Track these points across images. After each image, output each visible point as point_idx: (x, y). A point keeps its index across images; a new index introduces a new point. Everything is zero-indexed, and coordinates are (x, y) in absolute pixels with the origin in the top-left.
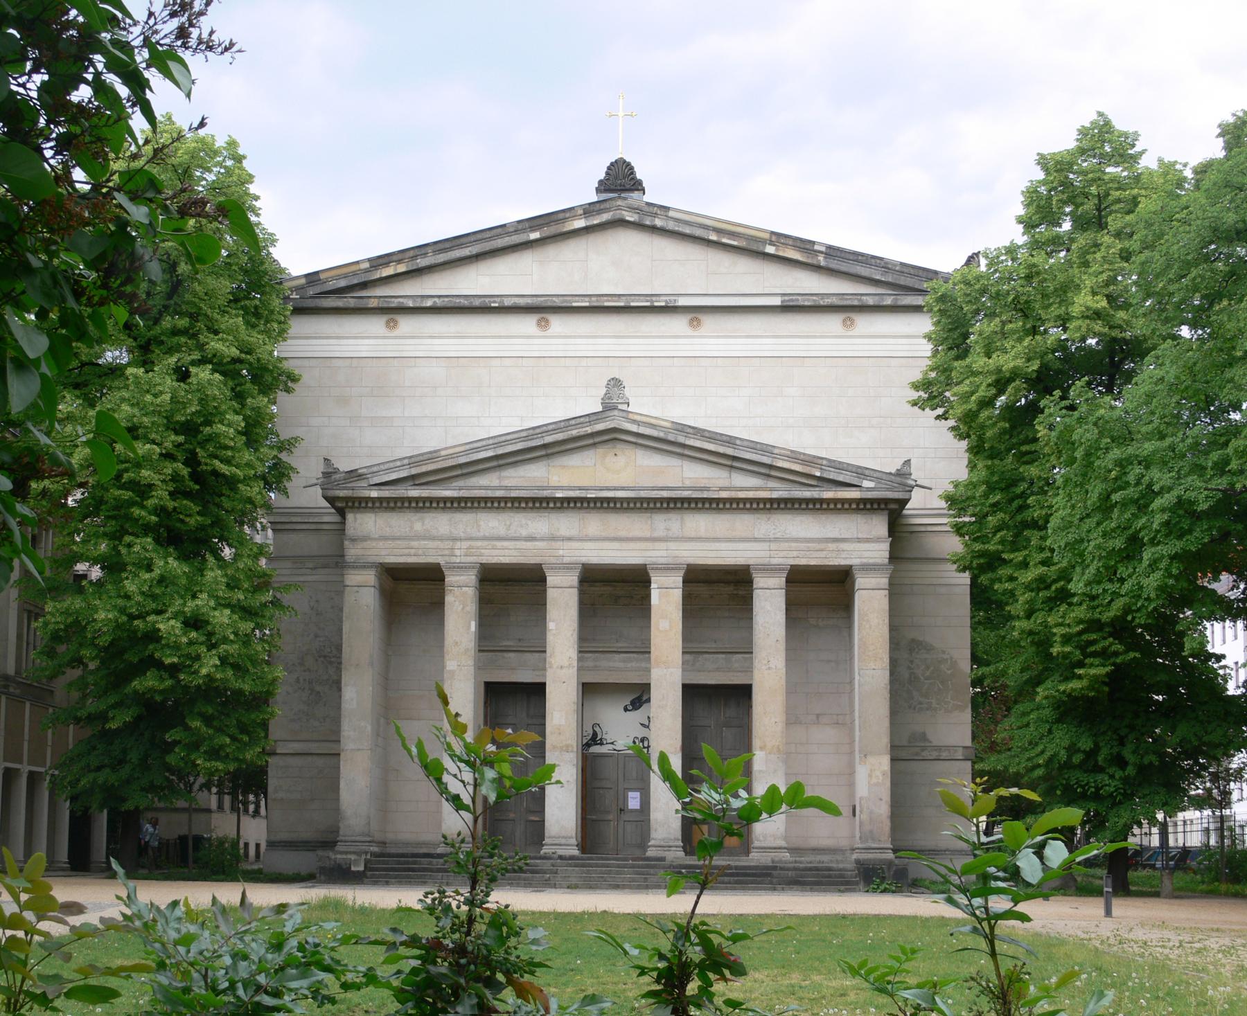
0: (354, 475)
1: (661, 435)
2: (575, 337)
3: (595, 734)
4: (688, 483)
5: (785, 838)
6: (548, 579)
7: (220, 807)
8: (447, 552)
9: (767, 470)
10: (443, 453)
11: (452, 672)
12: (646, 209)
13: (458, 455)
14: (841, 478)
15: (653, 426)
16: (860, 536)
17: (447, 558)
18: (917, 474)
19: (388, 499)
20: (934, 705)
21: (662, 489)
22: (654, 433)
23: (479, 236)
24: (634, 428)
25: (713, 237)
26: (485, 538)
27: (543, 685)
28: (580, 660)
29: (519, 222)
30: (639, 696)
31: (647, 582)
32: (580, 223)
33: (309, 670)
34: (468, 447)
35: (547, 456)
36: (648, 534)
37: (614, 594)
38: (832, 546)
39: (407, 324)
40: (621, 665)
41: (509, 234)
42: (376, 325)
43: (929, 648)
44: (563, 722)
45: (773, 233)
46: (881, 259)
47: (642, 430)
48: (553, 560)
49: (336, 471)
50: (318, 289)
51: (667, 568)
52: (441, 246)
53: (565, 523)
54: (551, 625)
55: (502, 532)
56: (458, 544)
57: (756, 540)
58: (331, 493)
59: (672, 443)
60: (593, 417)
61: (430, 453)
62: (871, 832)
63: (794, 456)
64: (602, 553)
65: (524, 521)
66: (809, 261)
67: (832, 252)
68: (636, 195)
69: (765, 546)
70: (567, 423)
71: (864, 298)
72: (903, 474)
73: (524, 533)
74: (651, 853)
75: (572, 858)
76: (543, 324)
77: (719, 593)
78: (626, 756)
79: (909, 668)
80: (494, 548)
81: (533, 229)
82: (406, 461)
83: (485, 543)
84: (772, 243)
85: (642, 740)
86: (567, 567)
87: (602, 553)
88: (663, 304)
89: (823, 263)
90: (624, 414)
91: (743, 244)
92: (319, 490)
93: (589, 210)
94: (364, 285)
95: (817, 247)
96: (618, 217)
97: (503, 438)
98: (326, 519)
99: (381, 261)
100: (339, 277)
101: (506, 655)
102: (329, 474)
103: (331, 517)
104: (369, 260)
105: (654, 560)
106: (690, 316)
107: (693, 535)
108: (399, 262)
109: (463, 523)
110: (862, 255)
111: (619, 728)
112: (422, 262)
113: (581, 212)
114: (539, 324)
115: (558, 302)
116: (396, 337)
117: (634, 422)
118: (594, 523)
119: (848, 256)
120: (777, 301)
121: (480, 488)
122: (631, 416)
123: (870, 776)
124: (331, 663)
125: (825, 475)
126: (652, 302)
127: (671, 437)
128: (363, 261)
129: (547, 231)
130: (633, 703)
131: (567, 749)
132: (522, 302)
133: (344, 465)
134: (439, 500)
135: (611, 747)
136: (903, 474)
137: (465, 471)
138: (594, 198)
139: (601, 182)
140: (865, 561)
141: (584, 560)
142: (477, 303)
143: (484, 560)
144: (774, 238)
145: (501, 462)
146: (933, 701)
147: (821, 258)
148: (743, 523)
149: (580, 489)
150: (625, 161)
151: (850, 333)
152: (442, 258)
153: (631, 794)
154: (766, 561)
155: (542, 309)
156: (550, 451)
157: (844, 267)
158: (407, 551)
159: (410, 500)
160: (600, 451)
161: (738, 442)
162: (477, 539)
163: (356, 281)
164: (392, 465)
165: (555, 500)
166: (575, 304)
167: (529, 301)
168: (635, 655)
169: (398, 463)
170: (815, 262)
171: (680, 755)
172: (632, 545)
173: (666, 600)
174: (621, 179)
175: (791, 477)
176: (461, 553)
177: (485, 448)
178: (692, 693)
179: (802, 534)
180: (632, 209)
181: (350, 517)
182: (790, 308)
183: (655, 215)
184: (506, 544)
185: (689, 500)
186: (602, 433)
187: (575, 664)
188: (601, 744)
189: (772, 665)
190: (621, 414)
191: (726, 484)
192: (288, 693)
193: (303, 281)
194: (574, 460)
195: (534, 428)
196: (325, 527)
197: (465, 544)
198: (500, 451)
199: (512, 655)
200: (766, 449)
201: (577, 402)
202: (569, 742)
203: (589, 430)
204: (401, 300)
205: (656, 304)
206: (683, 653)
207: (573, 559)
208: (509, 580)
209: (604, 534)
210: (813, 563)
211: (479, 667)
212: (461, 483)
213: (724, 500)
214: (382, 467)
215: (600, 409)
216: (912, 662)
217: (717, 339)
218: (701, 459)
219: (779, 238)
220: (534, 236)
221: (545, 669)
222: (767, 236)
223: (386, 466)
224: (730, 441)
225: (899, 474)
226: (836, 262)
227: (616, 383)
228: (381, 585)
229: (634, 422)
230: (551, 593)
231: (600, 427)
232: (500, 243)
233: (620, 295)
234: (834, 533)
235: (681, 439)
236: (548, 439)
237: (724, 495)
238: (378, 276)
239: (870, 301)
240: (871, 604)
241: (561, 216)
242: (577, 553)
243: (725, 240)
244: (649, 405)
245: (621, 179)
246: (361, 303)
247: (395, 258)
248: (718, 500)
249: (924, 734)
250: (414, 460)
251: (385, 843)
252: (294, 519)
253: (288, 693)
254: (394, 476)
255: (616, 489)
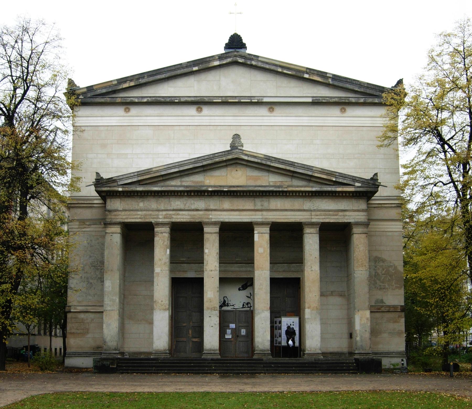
0: (111, 181)
1: (259, 161)
2: (214, 116)
3: (225, 301)
4: (271, 184)
5: (320, 350)
6: (205, 229)
7: (39, 334)
8: (155, 217)
9: (309, 178)
10: (154, 170)
11: (158, 274)
12: (248, 56)
13: (161, 170)
14: (345, 182)
15: (255, 157)
16: (354, 208)
17: (156, 220)
18: (381, 179)
19: (127, 192)
20: (387, 286)
21: (259, 186)
22: (256, 160)
23: (170, 69)
24: (246, 158)
25: (280, 70)
26: (174, 210)
27: (202, 279)
28: (220, 267)
29: (188, 62)
30: (247, 283)
31: (253, 231)
32: (217, 63)
33: (87, 272)
34: (166, 167)
35: (181, 176)
36: (253, 208)
37: (237, 237)
38: (340, 213)
39: (134, 110)
40: (237, 269)
41: (183, 68)
42: (120, 111)
43: (383, 261)
44: (212, 296)
45: (307, 68)
46: (358, 81)
47: (250, 159)
48: (207, 220)
49: (102, 178)
50: (93, 94)
51: (262, 224)
52: (151, 73)
53: (213, 203)
54: (206, 251)
55: (182, 207)
56: (161, 213)
57: (304, 210)
58: (99, 189)
59: (264, 165)
60: (228, 152)
61: (148, 169)
62: (361, 346)
63: (323, 171)
64: (231, 217)
65: (192, 202)
66: (325, 81)
67: (336, 78)
68: (242, 50)
69: (308, 213)
70: (214, 155)
71: (350, 99)
72: (374, 179)
73: (193, 207)
74: (255, 357)
75: (217, 360)
76: (200, 110)
77: (287, 237)
78: (240, 311)
79: (374, 270)
80: (178, 215)
81: (195, 66)
82: (136, 174)
83: (174, 212)
84: (307, 73)
85: (247, 304)
86: (215, 223)
87: (231, 217)
88: (256, 101)
89: (331, 83)
90: (241, 151)
91: (294, 73)
92: (93, 188)
93: (221, 57)
94: (114, 92)
95: (328, 75)
96: (234, 60)
97: (183, 163)
98: (95, 202)
99: (123, 80)
100: (102, 88)
101: (182, 265)
102: (99, 182)
103: (99, 201)
104: (117, 80)
105: (256, 220)
106: (269, 106)
107: (274, 208)
108: (131, 81)
109: (163, 203)
110: (349, 79)
111: (237, 299)
112: (142, 81)
113: (217, 58)
114: (197, 110)
115: (206, 100)
116: (129, 116)
117: (246, 155)
118: (227, 203)
119: (342, 79)
120: (310, 100)
121: (172, 186)
122: (244, 152)
123: (361, 320)
124: (98, 269)
125: (338, 180)
126: (251, 100)
127: (264, 162)
128: (114, 80)
129: (201, 67)
130: (243, 287)
131: (214, 309)
132: (189, 99)
133: (106, 176)
134: (151, 192)
135: (232, 307)
136: (374, 179)
137: (164, 178)
138: (223, 52)
139: (226, 44)
140: (356, 220)
141: (222, 220)
142: (168, 100)
143: (174, 220)
144: (308, 71)
145: (182, 174)
146: (386, 285)
147: (330, 80)
148: (297, 203)
149: (220, 186)
150: (237, 35)
151: (344, 115)
152: (151, 79)
153: (242, 330)
154: (309, 220)
155: (199, 103)
156: (205, 169)
157: (341, 84)
158: (136, 216)
159: (138, 192)
160: (229, 169)
161: (296, 165)
162: (170, 210)
163: (110, 90)
164: (129, 175)
165: (208, 191)
166: (214, 101)
167: (193, 99)
168: (244, 265)
169: (132, 175)
170: (327, 82)
171: (269, 311)
172: (245, 213)
173: (261, 240)
174: (236, 43)
175: (321, 181)
176: (161, 217)
177: (174, 167)
178: (274, 282)
179: (327, 208)
180: (241, 57)
181: (108, 201)
182: (317, 103)
183: (252, 59)
184: (184, 213)
185: (272, 192)
186: (234, 159)
187: (218, 269)
188: (228, 306)
189: (313, 269)
190: (240, 151)
191: (290, 183)
192: (77, 283)
193: (85, 90)
194: (217, 173)
195: (198, 158)
196: (95, 205)
197: (164, 213)
198: (182, 169)
199: (185, 265)
200: (309, 168)
201: (219, 146)
202: (216, 306)
203: (224, 159)
204: (132, 99)
205: (253, 101)
206: (270, 263)
207: (217, 220)
208: (263, 224)
209: (231, 208)
210: (332, 221)
211: (171, 271)
212: (162, 184)
213: (289, 192)
214: (124, 176)
215: (230, 149)
216: (376, 267)
217: (281, 118)
218: (277, 172)
219: (310, 71)
220: (195, 69)
221: (203, 271)
222: (305, 70)
223: (126, 176)
224: (292, 164)
225: (372, 179)
226: (337, 82)
227: (236, 137)
228: (122, 232)
229: (246, 155)
230: (206, 236)
231: (230, 157)
232: (179, 72)
233: (236, 97)
234: (342, 208)
235: (269, 163)
236: (205, 163)
237: (290, 189)
238: (121, 87)
239: (353, 100)
240: (359, 242)
241: (208, 59)
242: (219, 217)
243: (285, 71)
244: (254, 146)
245: (236, 43)
246: (113, 100)
247: (129, 79)
248: (286, 192)
249: (382, 300)
250: (140, 173)
251: (124, 353)
252: (80, 202)
253: (77, 283)
254: (130, 181)
255: (238, 187)
